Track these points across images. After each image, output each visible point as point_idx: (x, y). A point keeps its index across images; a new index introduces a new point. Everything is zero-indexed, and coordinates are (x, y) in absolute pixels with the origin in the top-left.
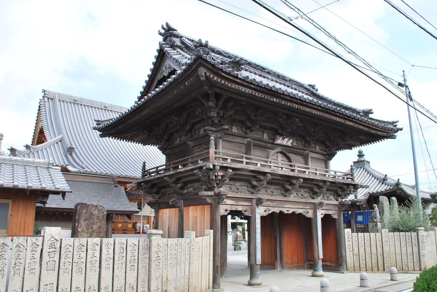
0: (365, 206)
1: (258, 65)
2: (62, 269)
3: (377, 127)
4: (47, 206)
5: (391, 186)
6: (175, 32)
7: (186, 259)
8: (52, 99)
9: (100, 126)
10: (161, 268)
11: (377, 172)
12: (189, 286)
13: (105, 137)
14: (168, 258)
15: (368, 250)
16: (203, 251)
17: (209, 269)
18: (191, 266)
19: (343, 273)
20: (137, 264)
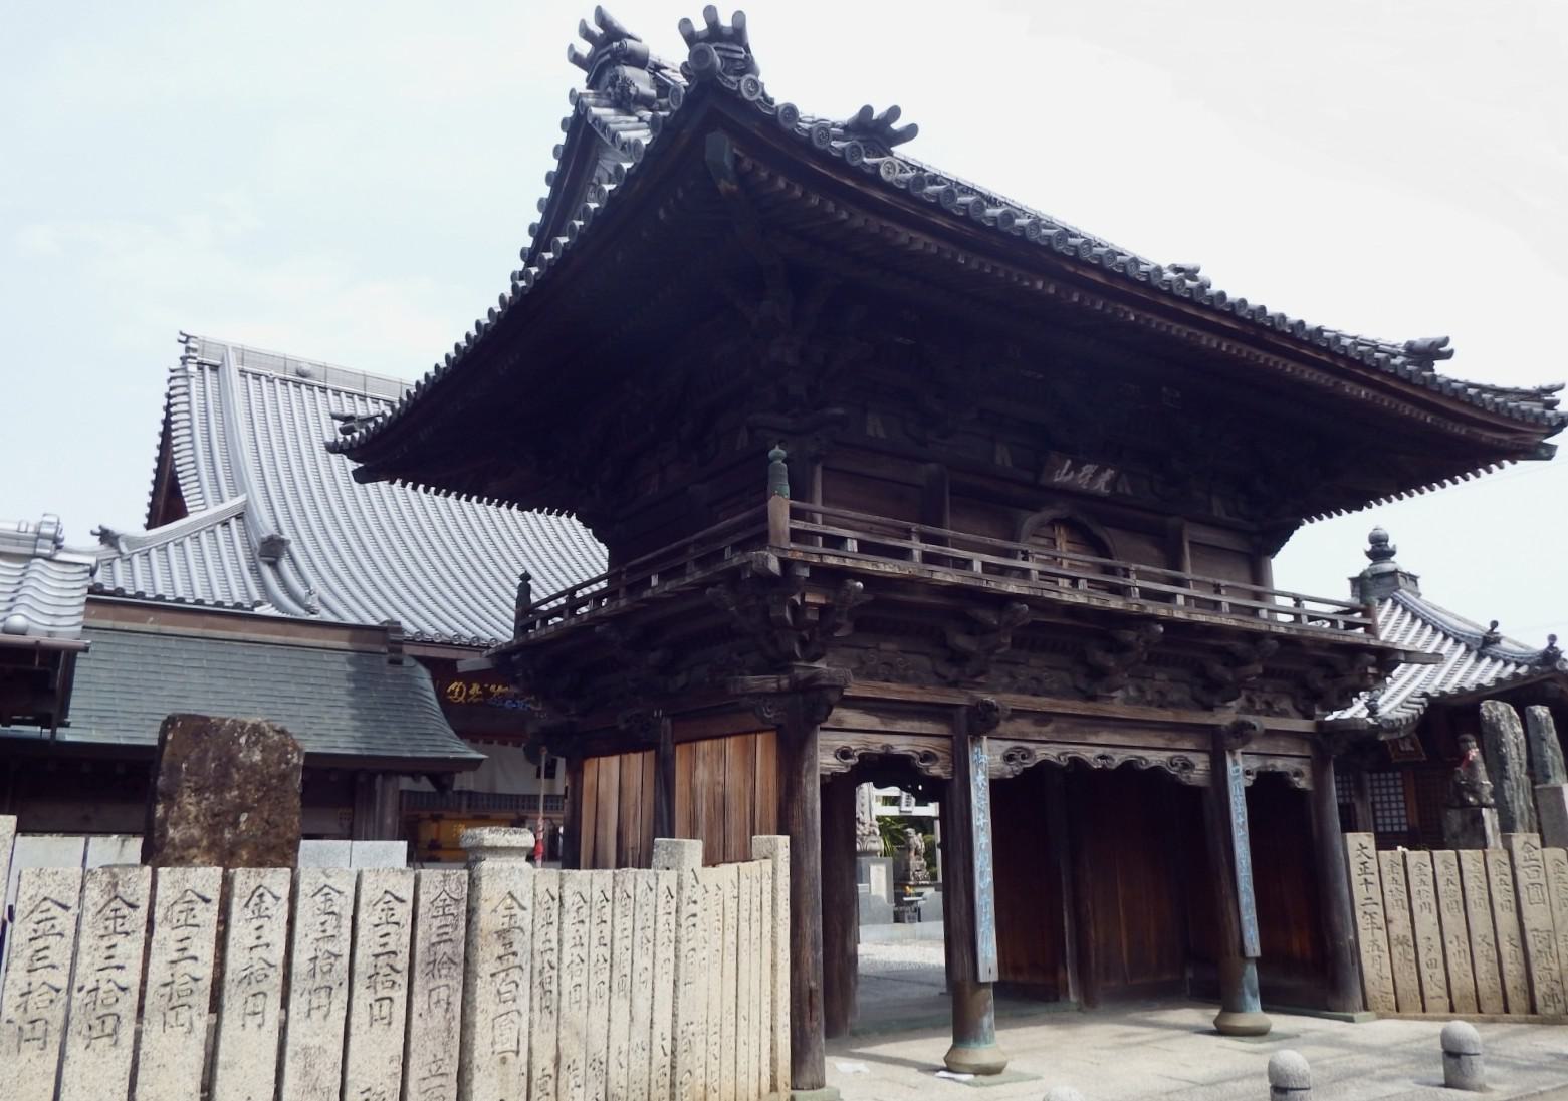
0: (1409, 747)
1: (969, 188)
2: (9, 1021)
3: (1476, 408)
4: (68, 735)
5: (1518, 666)
6: (630, 43)
7: (659, 963)
8: (214, 368)
9: (353, 437)
10: (525, 1009)
11: (1452, 615)
12: (672, 1085)
13: (375, 479)
14: (566, 960)
15: (1453, 922)
16: (744, 925)
17: (774, 1002)
18: (681, 994)
19: (1351, 1020)
20: (404, 991)
